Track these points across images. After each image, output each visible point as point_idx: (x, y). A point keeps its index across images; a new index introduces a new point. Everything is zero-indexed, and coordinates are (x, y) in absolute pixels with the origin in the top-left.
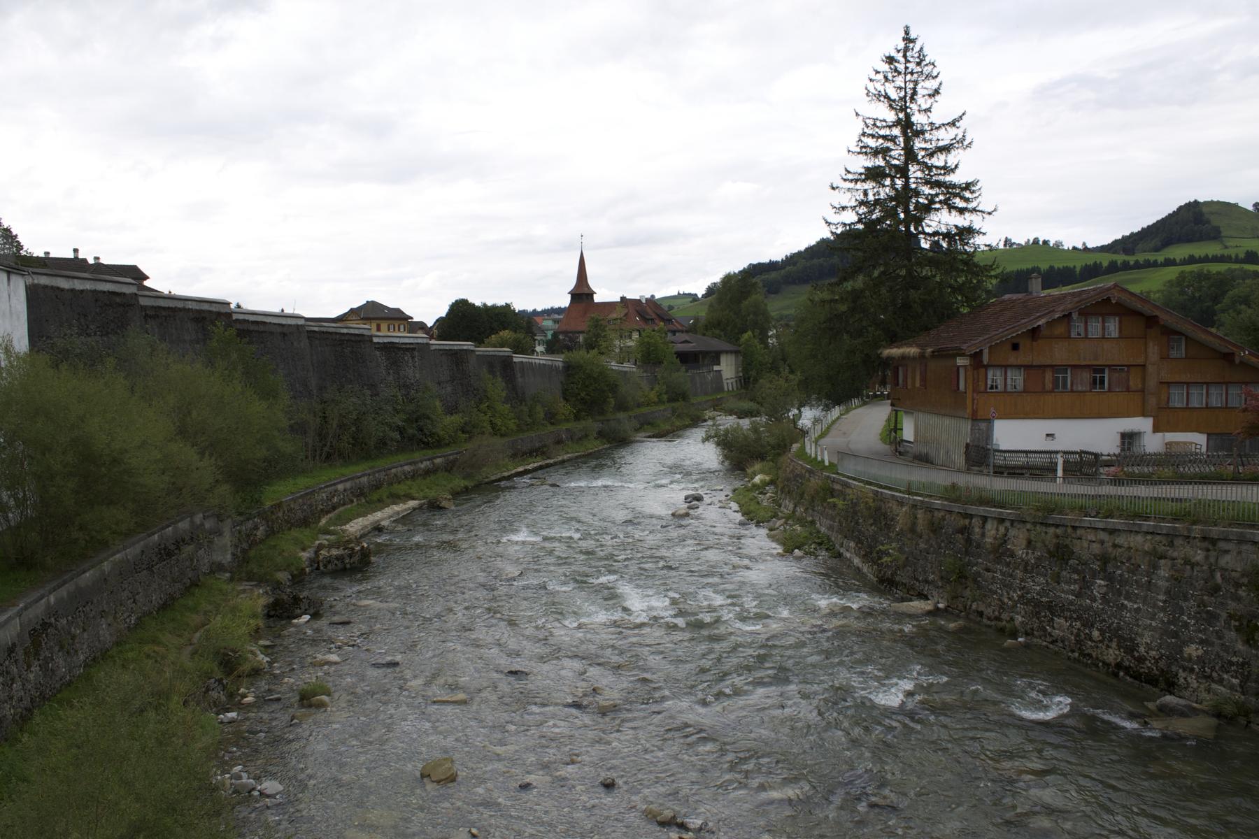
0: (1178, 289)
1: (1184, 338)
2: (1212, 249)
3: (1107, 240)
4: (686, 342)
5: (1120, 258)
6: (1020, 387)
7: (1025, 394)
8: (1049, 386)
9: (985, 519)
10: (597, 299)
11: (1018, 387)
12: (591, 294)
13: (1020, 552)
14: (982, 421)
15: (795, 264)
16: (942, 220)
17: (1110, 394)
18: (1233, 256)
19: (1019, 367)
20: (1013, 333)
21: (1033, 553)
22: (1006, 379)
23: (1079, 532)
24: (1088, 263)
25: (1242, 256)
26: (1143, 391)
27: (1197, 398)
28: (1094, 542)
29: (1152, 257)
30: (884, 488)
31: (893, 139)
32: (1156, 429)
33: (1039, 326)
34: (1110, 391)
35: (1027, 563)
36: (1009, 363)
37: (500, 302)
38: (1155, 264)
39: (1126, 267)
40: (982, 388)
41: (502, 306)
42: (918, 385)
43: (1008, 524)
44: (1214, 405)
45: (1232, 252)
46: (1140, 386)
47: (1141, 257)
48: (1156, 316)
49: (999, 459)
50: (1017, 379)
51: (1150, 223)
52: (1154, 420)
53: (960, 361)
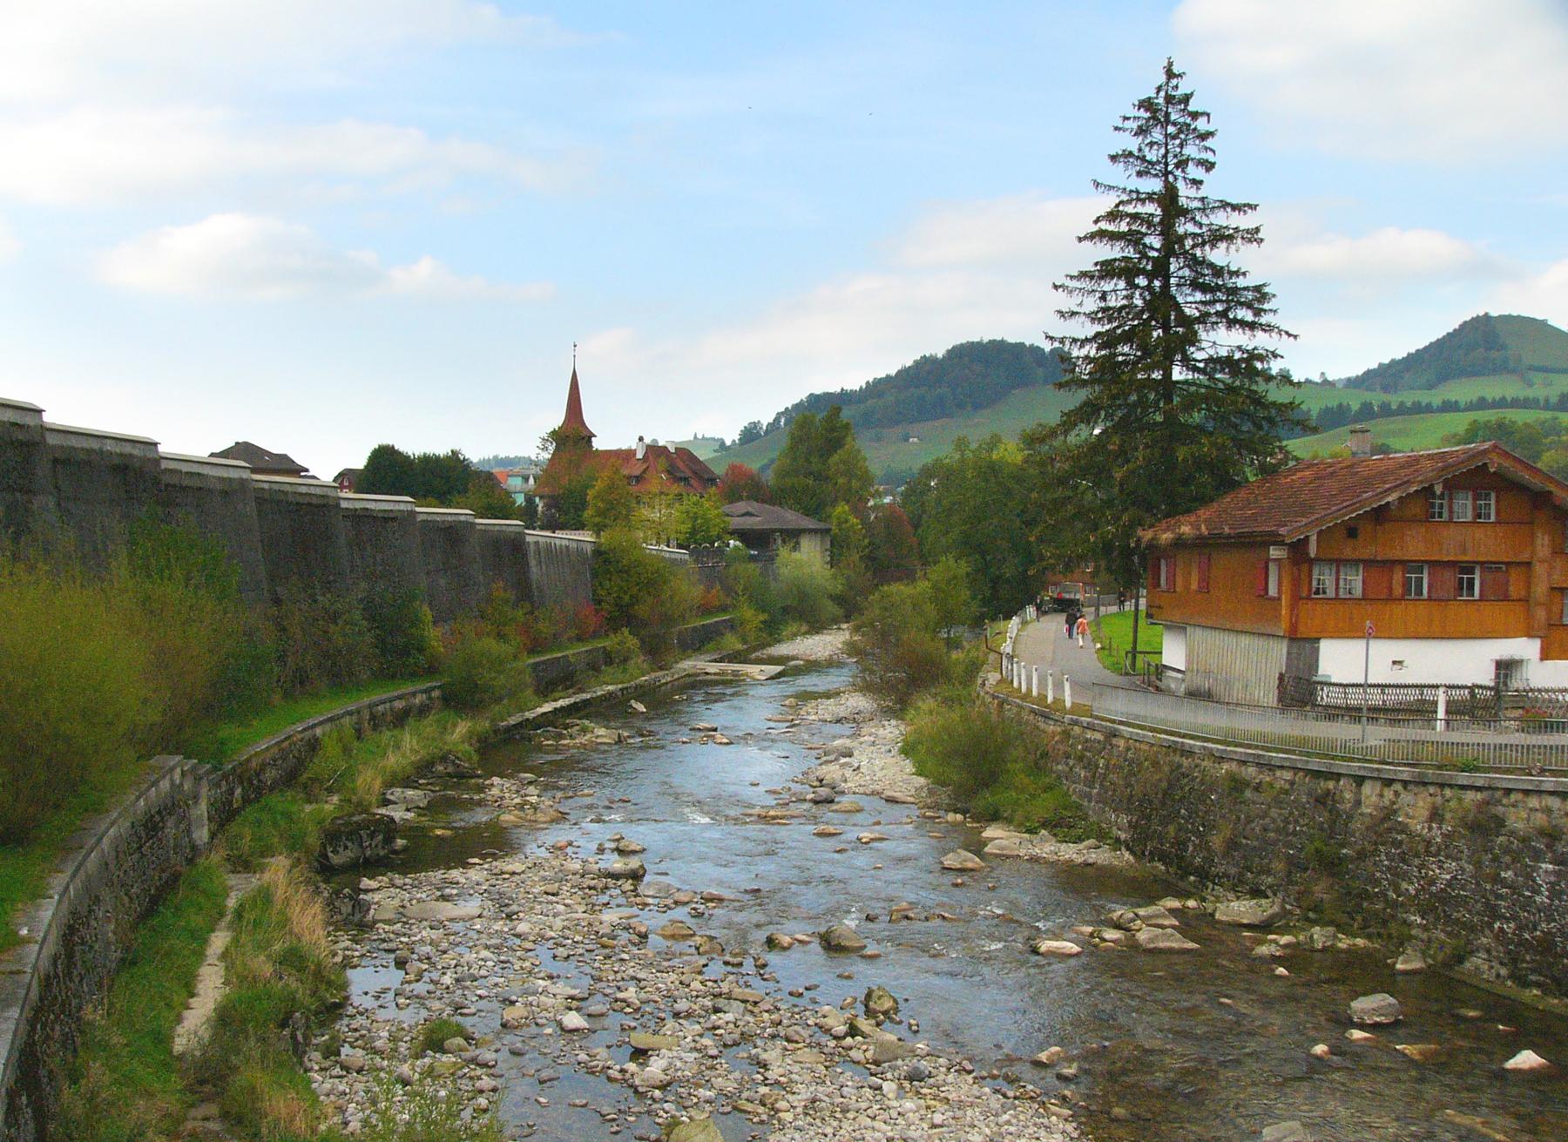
2: (1507, 388)
3: (1357, 370)
4: (748, 514)
5: (1376, 398)
6: (1358, 592)
7: (1363, 602)
9: (1360, 780)
10: (598, 444)
11: (1353, 591)
13: (1419, 827)
14: (1303, 643)
15: (880, 395)
16: (1220, 341)
18: (1542, 402)
20: (1352, 512)
21: (1440, 828)
22: (1337, 580)
23: (1513, 797)
24: (1330, 406)
25: (1554, 400)
26: (1525, 600)
28: (1537, 810)
29: (1424, 397)
30: (1171, 735)
31: (1147, 220)
32: (1545, 655)
33: (1388, 503)
34: (1481, 600)
35: (1429, 843)
36: (1343, 557)
37: (441, 450)
38: (1429, 409)
39: (1386, 411)
41: (447, 458)
42: (1194, 586)
43: (1398, 787)
46: (1523, 593)
47: (1408, 398)
49: (1326, 697)
51: (1421, 347)
52: (1542, 641)
53: (1274, 552)
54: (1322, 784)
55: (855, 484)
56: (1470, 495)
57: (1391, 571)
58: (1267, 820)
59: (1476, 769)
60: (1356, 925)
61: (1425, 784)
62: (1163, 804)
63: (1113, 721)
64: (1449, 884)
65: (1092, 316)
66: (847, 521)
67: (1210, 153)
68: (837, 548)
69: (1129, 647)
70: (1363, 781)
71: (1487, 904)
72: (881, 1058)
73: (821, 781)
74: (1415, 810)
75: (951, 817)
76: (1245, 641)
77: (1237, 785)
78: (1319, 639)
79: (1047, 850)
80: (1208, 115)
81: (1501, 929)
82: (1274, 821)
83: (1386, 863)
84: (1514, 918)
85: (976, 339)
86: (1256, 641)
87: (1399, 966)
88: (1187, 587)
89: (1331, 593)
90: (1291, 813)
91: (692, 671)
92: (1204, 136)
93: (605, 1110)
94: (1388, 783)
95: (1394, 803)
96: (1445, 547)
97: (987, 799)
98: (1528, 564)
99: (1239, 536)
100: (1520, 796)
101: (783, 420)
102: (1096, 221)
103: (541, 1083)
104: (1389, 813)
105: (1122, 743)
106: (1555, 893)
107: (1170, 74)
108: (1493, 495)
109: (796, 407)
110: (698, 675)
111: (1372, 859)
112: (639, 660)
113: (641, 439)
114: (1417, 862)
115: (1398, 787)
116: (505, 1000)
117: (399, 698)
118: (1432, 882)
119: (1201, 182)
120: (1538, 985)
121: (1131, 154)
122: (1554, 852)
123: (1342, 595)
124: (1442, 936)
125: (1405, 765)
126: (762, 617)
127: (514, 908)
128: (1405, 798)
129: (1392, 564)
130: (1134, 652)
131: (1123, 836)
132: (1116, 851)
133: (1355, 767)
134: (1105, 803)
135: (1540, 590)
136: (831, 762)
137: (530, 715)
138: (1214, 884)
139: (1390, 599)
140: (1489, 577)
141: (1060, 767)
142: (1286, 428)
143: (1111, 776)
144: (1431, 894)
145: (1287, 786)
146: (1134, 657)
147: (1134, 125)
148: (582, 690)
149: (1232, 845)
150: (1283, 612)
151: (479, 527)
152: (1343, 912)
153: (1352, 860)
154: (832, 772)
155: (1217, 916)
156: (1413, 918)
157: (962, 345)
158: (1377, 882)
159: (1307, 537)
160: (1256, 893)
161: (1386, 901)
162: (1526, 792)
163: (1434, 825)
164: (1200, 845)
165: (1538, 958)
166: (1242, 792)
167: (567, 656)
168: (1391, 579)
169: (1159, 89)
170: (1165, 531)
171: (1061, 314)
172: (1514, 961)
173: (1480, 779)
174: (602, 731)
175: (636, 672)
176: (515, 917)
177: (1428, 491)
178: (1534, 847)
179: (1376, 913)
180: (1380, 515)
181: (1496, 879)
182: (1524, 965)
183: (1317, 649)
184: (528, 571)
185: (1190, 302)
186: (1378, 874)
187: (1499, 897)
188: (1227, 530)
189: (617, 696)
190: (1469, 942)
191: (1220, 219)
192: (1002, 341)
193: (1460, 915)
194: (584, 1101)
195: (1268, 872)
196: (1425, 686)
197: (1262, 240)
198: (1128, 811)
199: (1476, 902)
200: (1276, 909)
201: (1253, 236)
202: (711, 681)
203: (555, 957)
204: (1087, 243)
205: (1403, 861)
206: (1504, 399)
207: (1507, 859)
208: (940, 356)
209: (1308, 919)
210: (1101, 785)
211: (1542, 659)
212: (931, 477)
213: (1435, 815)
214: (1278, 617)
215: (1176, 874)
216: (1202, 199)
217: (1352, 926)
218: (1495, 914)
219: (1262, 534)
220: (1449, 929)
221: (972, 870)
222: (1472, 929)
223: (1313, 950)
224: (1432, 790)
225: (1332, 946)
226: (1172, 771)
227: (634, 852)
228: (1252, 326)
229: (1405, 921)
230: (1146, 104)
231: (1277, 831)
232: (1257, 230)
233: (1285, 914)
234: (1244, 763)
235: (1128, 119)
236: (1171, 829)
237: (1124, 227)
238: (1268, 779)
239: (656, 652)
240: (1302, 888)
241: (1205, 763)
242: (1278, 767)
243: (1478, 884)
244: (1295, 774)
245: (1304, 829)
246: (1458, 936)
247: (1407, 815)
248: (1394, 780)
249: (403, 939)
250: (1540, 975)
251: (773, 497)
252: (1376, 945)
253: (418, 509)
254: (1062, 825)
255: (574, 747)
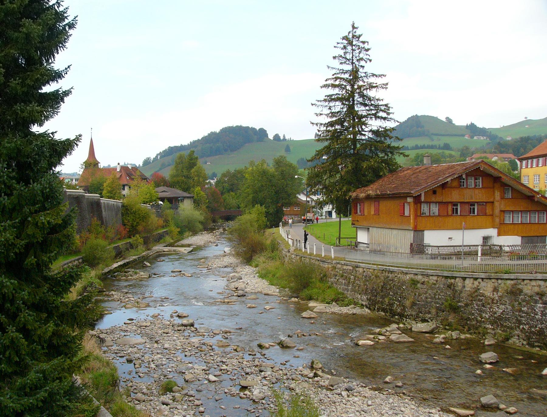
0: (416, 163)
1: (510, 188)
4: (164, 191)
6: (437, 214)
8: (450, 213)
9: (464, 279)
12: (96, 164)
13: (489, 294)
14: (418, 231)
16: (374, 124)
17: (478, 217)
19: (436, 203)
20: (435, 185)
23: (526, 282)
25: (442, 145)
27: (518, 219)
32: (499, 234)
34: (478, 215)
35: (493, 300)
36: (432, 201)
40: (419, 214)
42: (373, 213)
44: (524, 222)
45: (435, 143)
48: (501, 177)
49: (430, 251)
50: (435, 209)
54: (449, 281)
55: (201, 179)
56: (473, 178)
57: (448, 206)
58: (427, 295)
59: (510, 273)
60: (465, 330)
61: (490, 279)
62: (382, 291)
63: (356, 262)
64: (502, 313)
65: (327, 115)
66: (200, 194)
67: (368, 56)
68: (197, 203)
69: (338, 236)
70: (465, 279)
71: (517, 320)
72: (333, 384)
73: (237, 288)
74: (487, 288)
75: (293, 299)
76: (395, 232)
77: (414, 283)
78: (424, 230)
79: (337, 309)
80: (368, 42)
81: (523, 328)
82: (430, 295)
83: (476, 307)
84: (527, 324)
85: (231, 125)
86: (400, 232)
87: (486, 343)
88: (369, 212)
89: (428, 214)
90: (437, 292)
91: (158, 251)
92: (367, 50)
93: (249, 409)
94: (476, 279)
95: (478, 286)
96: (465, 197)
97: (306, 293)
98: (493, 202)
99: (394, 194)
100: (528, 281)
101: (159, 157)
102: (326, 80)
103: (216, 401)
104: (477, 289)
105: (361, 270)
106: (543, 314)
107: (354, 27)
108: (481, 178)
109: (164, 151)
110: (161, 252)
111: (471, 306)
112: (141, 247)
113: (119, 164)
114: (488, 306)
115: (480, 280)
116: (180, 372)
117: (70, 262)
118: (495, 313)
119: (364, 67)
120: (538, 346)
121: (341, 56)
122: (542, 300)
123: (431, 215)
124: (500, 332)
125: (482, 272)
126: (179, 230)
127: (157, 339)
128: (483, 284)
129: (448, 203)
130: (340, 238)
131: (364, 303)
132: (362, 308)
133: (463, 274)
134: (355, 291)
135: (497, 211)
136: (235, 281)
137: (110, 268)
138: (406, 318)
139: (448, 215)
140: (480, 207)
141: (332, 280)
142: (397, 155)
143: (357, 282)
144: (495, 317)
145: (435, 282)
146: (340, 240)
147: (342, 46)
148: (124, 259)
149: (413, 304)
150: (412, 221)
151: (86, 197)
152: (460, 325)
153: (463, 307)
154: (236, 284)
155: (413, 329)
156: (488, 326)
157: (226, 128)
158: (473, 314)
159: (421, 194)
160: (424, 321)
161: (477, 321)
162: (531, 280)
163: (495, 293)
164: (399, 305)
165: (538, 337)
166: (416, 285)
167: (119, 246)
168: (448, 208)
169: (349, 33)
170: (361, 193)
171: (317, 115)
172: (529, 339)
173: (512, 276)
174: (142, 273)
175: (141, 251)
176: (159, 342)
177: (460, 177)
178: (535, 299)
179: (473, 325)
180: (444, 186)
181: (520, 311)
182: (533, 340)
183: (423, 235)
184: (102, 214)
185: (360, 109)
186: (473, 312)
187: (521, 317)
188: (388, 192)
189: (137, 261)
190: (510, 333)
191: (372, 80)
192: (241, 126)
193: (507, 324)
194: (239, 406)
195: (429, 313)
196: (472, 246)
197: (387, 88)
198: (366, 294)
199: (513, 319)
200: (434, 326)
201: (385, 86)
202: (165, 254)
203: (186, 356)
204: (324, 89)
205: (483, 306)
206: (424, 145)
207: (524, 303)
208: (218, 132)
209: (445, 329)
210: (353, 285)
211: (498, 236)
212: (226, 177)
213: (495, 290)
214: (409, 223)
215: (390, 316)
216: (365, 73)
217: (464, 330)
218: (520, 322)
219: (403, 193)
220: (503, 329)
221: (313, 318)
222: (512, 328)
223: (452, 339)
224: (493, 280)
225: (459, 338)
226: (385, 279)
227: (185, 317)
228: (385, 119)
229: (485, 327)
230: (345, 38)
231: (431, 298)
232: (387, 84)
233: (437, 327)
234: (417, 274)
235: (339, 43)
236: (387, 300)
237: (337, 83)
238: (427, 280)
239: (146, 242)
240: (443, 318)
241: (399, 276)
242: (431, 275)
243: (513, 312)
244: (438, 278)
245: (443, 297)
246: (506, 331)
247: (484, 290)
248: (478, 278)
249: (124, 352)
250: (539, 343)
251: (171, 185)
252: (474, 336)
253: (67, 190)
254: (338, 300)
255: (134, 279)
